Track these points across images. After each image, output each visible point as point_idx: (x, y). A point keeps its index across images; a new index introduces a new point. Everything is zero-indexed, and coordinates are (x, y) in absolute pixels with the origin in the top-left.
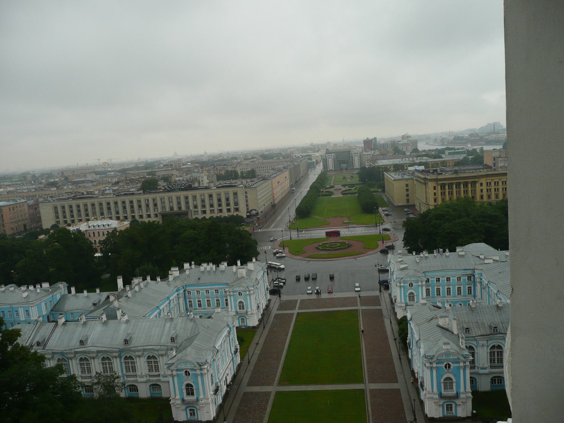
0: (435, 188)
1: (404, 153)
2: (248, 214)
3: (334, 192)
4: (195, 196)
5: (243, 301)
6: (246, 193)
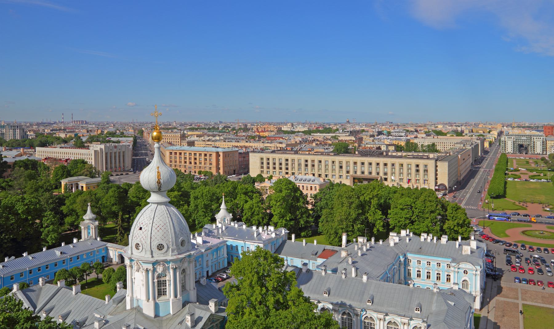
2: (437, 188)
4: (402, 165)
5: (467, 279)
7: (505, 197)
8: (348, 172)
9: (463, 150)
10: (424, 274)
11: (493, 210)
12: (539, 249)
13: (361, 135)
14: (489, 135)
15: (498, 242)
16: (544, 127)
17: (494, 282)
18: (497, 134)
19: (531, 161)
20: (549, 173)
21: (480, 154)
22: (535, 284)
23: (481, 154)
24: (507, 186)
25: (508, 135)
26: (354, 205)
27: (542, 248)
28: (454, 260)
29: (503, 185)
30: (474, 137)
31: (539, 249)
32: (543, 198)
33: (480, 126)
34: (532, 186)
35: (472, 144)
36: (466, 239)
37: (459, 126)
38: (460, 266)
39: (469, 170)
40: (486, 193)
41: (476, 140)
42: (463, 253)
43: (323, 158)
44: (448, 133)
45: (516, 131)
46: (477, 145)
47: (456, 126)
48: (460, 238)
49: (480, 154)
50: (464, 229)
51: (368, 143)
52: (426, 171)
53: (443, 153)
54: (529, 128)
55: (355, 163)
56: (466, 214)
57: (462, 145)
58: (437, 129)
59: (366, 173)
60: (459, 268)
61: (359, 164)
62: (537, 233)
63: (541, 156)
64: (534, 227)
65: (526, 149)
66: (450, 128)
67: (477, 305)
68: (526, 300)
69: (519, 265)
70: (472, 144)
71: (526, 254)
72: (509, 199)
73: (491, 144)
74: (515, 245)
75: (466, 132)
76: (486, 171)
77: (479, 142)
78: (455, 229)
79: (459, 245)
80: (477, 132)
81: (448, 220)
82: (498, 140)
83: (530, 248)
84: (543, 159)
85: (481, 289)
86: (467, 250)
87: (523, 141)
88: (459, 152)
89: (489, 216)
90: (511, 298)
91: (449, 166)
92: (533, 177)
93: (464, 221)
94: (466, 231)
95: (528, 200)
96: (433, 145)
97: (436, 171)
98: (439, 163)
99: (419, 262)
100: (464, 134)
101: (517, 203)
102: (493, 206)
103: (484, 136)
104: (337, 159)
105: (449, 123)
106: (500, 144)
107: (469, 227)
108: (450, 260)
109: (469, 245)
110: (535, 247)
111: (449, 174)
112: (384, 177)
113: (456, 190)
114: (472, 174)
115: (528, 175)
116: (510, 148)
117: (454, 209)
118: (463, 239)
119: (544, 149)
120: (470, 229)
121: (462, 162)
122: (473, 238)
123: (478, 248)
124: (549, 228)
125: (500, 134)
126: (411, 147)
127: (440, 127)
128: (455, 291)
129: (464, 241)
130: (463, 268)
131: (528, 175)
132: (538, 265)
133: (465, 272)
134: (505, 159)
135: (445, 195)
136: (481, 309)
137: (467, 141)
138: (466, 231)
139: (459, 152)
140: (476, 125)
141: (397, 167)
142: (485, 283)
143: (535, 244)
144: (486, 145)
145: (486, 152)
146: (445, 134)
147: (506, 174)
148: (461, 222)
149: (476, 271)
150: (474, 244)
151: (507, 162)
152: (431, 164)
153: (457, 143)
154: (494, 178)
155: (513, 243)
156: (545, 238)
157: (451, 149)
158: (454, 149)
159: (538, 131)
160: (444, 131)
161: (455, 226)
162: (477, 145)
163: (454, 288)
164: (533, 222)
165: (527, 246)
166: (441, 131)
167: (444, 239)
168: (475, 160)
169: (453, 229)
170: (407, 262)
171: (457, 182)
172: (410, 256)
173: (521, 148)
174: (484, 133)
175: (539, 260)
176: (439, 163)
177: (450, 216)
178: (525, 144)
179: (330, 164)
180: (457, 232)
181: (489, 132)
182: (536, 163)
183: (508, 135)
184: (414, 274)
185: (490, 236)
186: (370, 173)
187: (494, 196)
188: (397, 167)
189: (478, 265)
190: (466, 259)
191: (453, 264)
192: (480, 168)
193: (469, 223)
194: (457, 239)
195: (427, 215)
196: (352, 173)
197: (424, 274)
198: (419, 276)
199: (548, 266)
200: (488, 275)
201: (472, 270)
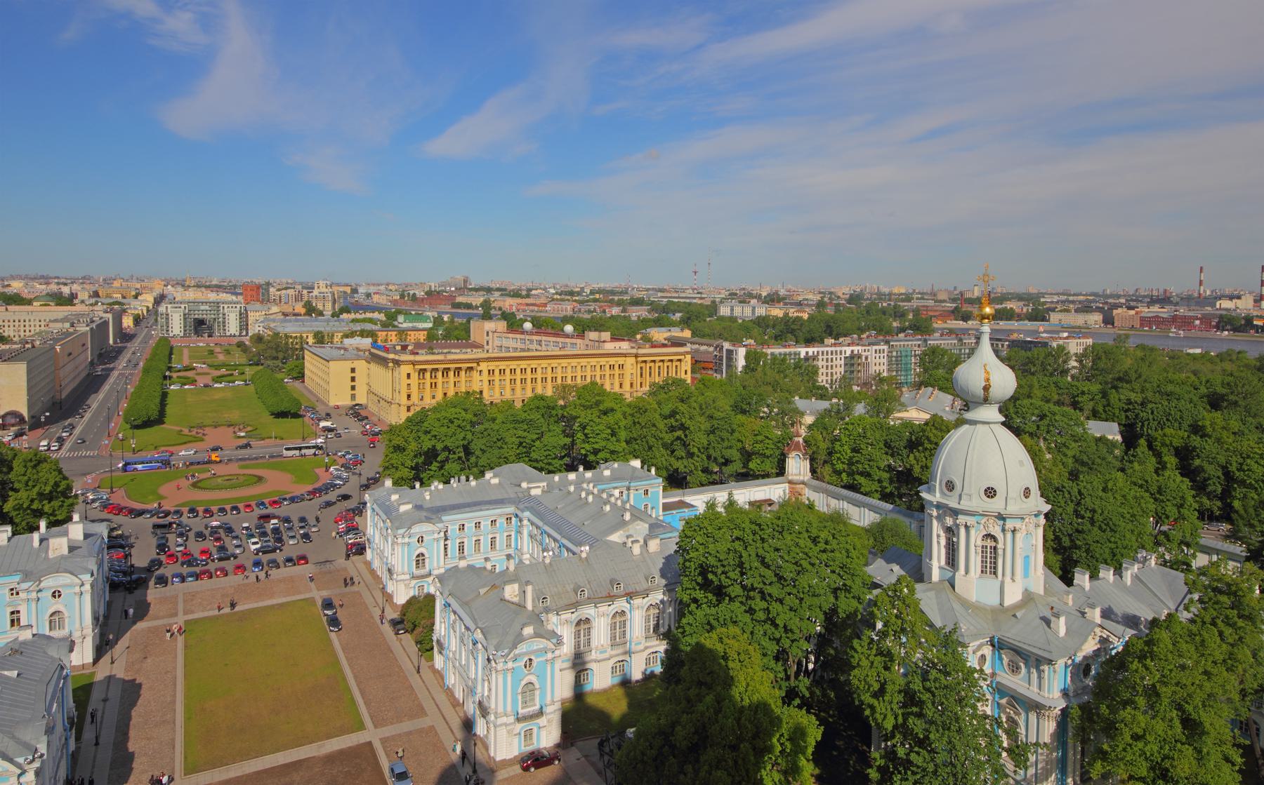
0: (409, 375)
1: (321, 314)
3: (197, 377)
5: (61, 608)
6: (353, 370)
7: (163, 423)
9: (67, 334)
11: (134, 451)
12: (222, 510)
14: (134, 303)
15: (140, 513)
16: (245, 286)
17: (128, 596)
18: (152, 300)
19: (218, 349)
20: (247, 369)
21: (111, 342)
22: (211, 577)
23: (115, 342)
24: (169, 400)
25: (173, 301)
27: (201, 509)
28: (27, 576)
29: (158, 400)
30: (99, 307)
31: (222, 510)
32: (235, 416)
33: (116, 284)
34: (217, 396)
35: (92, 322)
36: (58, 523)
37: (65, 284)
38: (42, 585)
39: (83, 375)
40: (121, 420)
41: (100, 313)
42: (1101, 566)
44: (36, 298)
45: (191, 295)
46: (106, 323)
47: (58, 284)
48: (43, 524)
49: (111, 342)
50: (56, 503)
53: (15, 343)
54: (218, 288)
56: (60, 471)
57: (67, 325)
58: (6, 290)
60: (40, 591)
62: (219, 480)
63: (236, 340)
64: (214, 469)
65: (210, 328)
66: (41, 288)
67: (82, 655)
68: (192, 612)
69: (181, 548)
70: (92, 322)
71: (196, 524)
72: (169, 426)
73: (137, 320)
74: (177, 512)
75: (83, 295)
76: (124, 377)
77: (110, 316)
78: (34, 506)
79: (41, 541)
80: (108, 296)
81: (16, 491)
82: (153, 312)
83: (206, 511)
84: (240, 345)
85: (96, 618)
86: (58, 546)
87: (203, 312)
88: (56, 340)
89: (126, 465)
90: (163, 618)
91: (29, 372)
92: (218, 379)
93: (57, 484)
94: (61, 506)
95: (207, 422)
100: (76, 301)
101: (186, 431)
102: (133, 443)
103: (123, 304)
105: (42, 277)
106: (156, 320)
107: (68, 498)
108: (17, 578)
109: (66, 534)
110: (215, 509)
111: (29, 389)
113: (50, 421)
114: (92, 383)
115: (210, 377)
116: (177, 327)
117: (29, 464)
118: (50, 525)
119: (244, 325)
120: (71, 501)
121: (67, 359)
122: (76, 517)
123: (86, 536)
124: (242, 467)
125: (160, 300)
127: (16, 286)
128: (24, 643)
129: (55, 529)
130: (50, 588)
131: (210, 377)
132: (218, 539)
133: (56, 594)
134: (167, 349)
135: (19, 435)
136: (96, 661)
137: (79, 315)
138: (61, 506)
139: (56, 340)
140: (108, 282)
142: (109, 605)
143: (215, 502)
144: (128, 322)
145: (126, 337)
146: (29, 302)
147: (165, 378)
148: (48, 489)
149: (83, 585)
150: (76, 530)
151: (171, 354)
153: (56, 321)
154: (140, 388)
155: (172, 510)
156: (232, 487)
157: (40, 333)
158: (47, 332)
159: (233, 294)
160: (26, 294)
161: (32, 501)
162: (106, 323)
163: (21, 639)
164: (216, 462)
165: (201, 509)
166: (17, 295)
168: (100, 355)
169: (28, 508)
171: (54, 404)
173: (199, 326)
174: (124, 297)
175: (221, 531)
177: (19, 481)
178: (208, 317)
180: (39, 514)
181: (136, 297)
182: (228, 352)
183: (173, 301)
185: (123, 504)
187: (139, 422)
189: (86, 570)
190: (58, 567)
191: (24, 586)
192: (113, 369)
193: (69, 488)
194: (38, 528)
199: (237, 537)
200: (114, 586)
201: (71, 586)
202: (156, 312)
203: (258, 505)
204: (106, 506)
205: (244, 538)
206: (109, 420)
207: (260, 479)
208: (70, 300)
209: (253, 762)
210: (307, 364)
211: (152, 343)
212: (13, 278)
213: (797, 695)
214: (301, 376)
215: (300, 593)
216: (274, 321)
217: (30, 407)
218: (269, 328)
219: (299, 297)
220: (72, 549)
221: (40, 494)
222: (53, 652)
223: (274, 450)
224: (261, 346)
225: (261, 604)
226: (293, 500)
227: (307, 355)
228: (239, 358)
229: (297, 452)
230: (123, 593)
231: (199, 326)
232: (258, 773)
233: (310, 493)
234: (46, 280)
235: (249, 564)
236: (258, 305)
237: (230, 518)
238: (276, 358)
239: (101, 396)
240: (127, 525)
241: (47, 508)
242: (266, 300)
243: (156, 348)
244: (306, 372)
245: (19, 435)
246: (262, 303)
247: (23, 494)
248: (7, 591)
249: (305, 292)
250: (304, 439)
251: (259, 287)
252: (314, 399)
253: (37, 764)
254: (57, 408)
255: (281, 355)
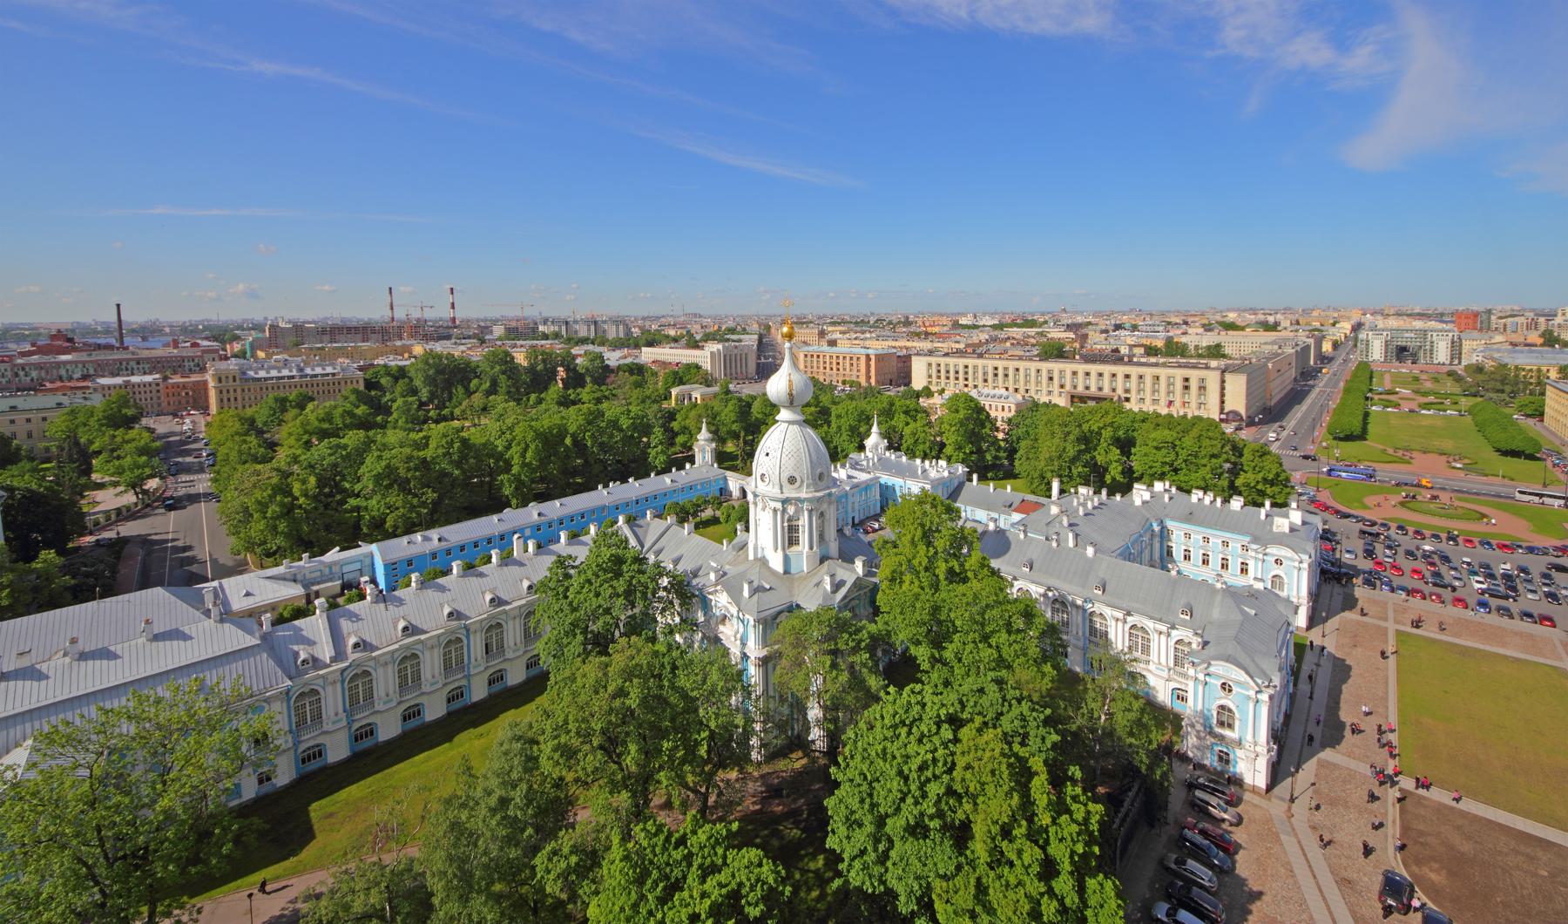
8: (1062, 386)
10: (1196, 556)
11: (1337, 460)
13: (1084, 331)
15: (1347, 516)
19: (1424, 377)
24: (1370, 419)
25: (1374, 328)
26: (1072, 437)
28: (1255, 540)
32: (1448, 445)
33: (1315, 314)
41: (1303, 338)
43: (1022, 365)
45: (1393, 323)
46: (1308, 347)
48: (1267, 504)
50: (1276, 489)
51: (1097, 342)
52: (1202, 388)
54: (1422, 316)
55: (1075, 373)
59: (1093, 389)
61: (1081, 375)
63: (1446, 369)
67: (1301, 620)
71: (1407, 542)
73: (1336, 345)
74: (1383, 525)
75: (1285, 323)
76: (1326, 392)
77: (1311, 341)
80: (1308, 324)
83: (1417, 532)
85: (1310, 593)
86: (1281, 524)
88: (1268, 359)
92: (1427, 406)
93: (1278, 475)
96: (1218, 346)
97: (1223, 388)
98: (1228, 377)
99: (1188, 536)
102: (1337, 453)
104: (1045, 366)
109: (1287, 516)
110: (1427, 533)
111: (1248, 395)
112: (1124, 395)
113: (1261, 422)
114: (1295, 396)
116: (1377, 352)
118: (1273, 505)
119: (1456, 350)
123: (1304, 523)
125: (1357, 327)
126: (1174, 349)
127: (1232, 317)
128: (1258, 591)
132: (1433, 564)
133: (1278, 562)
134: (1366, 372)
135: (1238, 429)
137: (1285, 340)
139: (1268, 359)
141: (1148, 380)
145: (1325, 359)
146: (1243, 329)
148: (1271, 477)
150: (1296, 517)
152: (1212, 379)
154: (1342, 404)
160: (1239, 322)
162: (1308, 347)
167: (1236, 503)
168: (1302, 373)
170: (1165, 534)
172: (1170, 524)
176: (1228, 377)
179: (1033, 373)
180: (1262, 494)
182: (1436, 380)
183: (1374, 328)
184: (1178, 554)
186: (1100, 389)
188: (1148, 380)
189: (1305, 552)
190: (1280, 540)
191: (1254, 546)
194: (1262, 505)
195: (1204, 461)
196: (1068, 387)
197: (1196, 556)
198: (1187, 558)
199: (1455, 569)
202: (1356, 339)
203: (1482, 543)
204: (1312, 501)
205: (1465, 573)
206: (1313, 428)
207: (1484, 516)
208: (1274, 327)
209: (1482, 806)
210: (1548, 401)
211: (1352, 366)
212: (1229, 310)
213: (566, 397)
214: (1540, 415)
215: (1544, 656)
216: (1498, 351)
217: (1248, 408)
218: (1493, 359)
219: (1532, 325)
220: (1292, 530)
221: (1265, 480)
222: (1281, 608)
223: (1504, 491)
224: (1481, 377)
225: (1488, 648)
226: (1531, 550)
227: (1550, 391)
228: (1450, 386)
229: (1536, 499)
230: (1332, 581)
231: (1401, 352)
232: (1490, 822)
233: (1556, 549)
234: (1254, 311)
235: (1472, 601)
236: (1475, 334)
237: (1447, 547)
238: (1502, 391)
239: (1304, 406)
240: (1336, 524)
241: (1269, 491)
242: (1486, 328)
243: (1355, 375)
244: (1547, 410)
245: (1238, 429)
246: (1481, 330)
247: (1250, 475)
248: (448, 287)
249: (1542, 320)
250: (1545, 485)
251: (1476, 315)
252: (1557, 442)
253: (1271, 691)
254: (1269, 413)
255: (1508, 389)
